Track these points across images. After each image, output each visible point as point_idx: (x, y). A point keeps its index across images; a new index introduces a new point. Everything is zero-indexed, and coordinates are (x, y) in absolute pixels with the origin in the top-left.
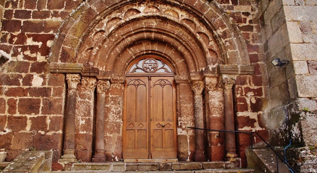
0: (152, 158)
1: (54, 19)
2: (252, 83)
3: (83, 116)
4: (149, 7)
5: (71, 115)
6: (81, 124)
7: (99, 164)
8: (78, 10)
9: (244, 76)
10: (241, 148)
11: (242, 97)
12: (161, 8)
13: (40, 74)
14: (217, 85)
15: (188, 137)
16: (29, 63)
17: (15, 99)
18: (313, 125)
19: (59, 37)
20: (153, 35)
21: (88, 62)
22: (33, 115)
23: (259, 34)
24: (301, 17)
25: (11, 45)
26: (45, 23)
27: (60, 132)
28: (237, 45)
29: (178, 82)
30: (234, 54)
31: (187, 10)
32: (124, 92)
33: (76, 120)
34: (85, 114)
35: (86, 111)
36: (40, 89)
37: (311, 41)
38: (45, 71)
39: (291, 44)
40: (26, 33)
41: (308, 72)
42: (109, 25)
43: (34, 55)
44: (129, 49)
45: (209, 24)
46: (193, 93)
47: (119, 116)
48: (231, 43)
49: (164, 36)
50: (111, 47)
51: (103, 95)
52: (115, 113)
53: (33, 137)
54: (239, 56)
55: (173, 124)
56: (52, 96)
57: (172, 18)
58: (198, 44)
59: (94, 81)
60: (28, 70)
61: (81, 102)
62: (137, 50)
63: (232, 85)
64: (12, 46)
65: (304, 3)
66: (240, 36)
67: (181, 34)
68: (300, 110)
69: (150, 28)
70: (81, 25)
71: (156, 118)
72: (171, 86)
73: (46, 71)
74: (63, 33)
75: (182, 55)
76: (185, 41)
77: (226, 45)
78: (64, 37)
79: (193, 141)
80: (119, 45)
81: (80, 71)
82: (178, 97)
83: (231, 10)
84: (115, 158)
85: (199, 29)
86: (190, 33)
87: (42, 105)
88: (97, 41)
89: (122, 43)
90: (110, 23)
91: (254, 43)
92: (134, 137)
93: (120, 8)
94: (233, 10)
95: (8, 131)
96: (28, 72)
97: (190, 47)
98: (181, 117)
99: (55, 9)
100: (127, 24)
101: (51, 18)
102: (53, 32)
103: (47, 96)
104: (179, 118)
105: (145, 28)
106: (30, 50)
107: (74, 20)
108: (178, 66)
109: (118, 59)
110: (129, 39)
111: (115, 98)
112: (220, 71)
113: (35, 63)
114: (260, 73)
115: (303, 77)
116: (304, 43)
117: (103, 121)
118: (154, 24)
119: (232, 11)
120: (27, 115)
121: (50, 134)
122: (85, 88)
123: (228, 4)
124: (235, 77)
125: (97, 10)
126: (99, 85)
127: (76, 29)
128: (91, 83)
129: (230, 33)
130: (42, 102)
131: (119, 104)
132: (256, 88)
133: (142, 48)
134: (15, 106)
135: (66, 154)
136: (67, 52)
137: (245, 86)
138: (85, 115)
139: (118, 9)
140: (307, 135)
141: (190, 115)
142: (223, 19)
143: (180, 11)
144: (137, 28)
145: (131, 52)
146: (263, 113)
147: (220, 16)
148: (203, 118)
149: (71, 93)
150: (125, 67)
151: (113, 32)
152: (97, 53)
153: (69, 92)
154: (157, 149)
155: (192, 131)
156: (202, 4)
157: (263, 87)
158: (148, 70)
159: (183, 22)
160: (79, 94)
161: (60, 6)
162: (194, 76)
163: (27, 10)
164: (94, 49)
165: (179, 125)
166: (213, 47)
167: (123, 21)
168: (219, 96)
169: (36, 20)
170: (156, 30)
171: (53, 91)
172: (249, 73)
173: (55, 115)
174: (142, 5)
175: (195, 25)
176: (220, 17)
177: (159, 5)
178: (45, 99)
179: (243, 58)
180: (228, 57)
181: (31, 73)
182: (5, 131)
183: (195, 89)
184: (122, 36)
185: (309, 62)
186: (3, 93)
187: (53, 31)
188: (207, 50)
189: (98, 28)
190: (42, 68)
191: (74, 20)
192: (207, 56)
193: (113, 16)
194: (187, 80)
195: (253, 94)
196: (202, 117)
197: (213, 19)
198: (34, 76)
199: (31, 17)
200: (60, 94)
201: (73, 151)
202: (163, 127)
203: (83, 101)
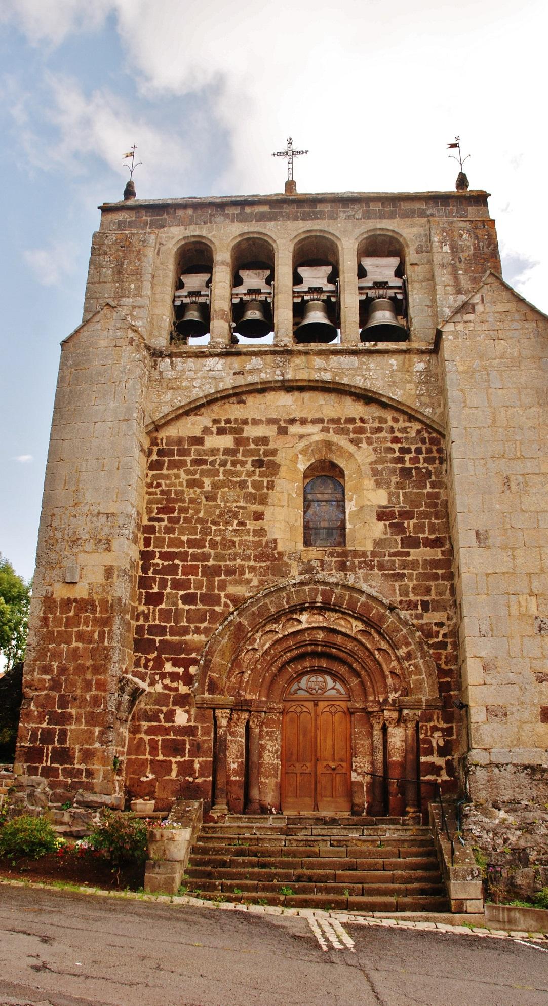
1: (196, 637)
2: (440, 720)
4: (314, 614)
6: (232, 768)
7: (256, 816)
8: (225, 626)
10: (423, 801)
12: (328, 616)
15: (365, 784)
16: (170, 695)
17: (157, 739)
20: (319, 649)
22: (179, 759)
23: (455, 653)
24: (486, 652)
26: (186, 642)
27: (211, 778)
28: (424, 670)
30: (419, 683)
31: (363, 621)
34: (236, 756)
35: (238, 752)
36: (185, 727)
37: (493, 682)
38: (190, 705)
39: (470, 687)
43: (175, 685)
44: (289, 665)
46: (372, 727)
48: (416, 667)
54: (426, 685)
57: (343, 630)
59: (245, 715)
61: (232, 741)
70: (229, 645)
74: (209, 657)
75: (358, 675)
78: (210, 661)
85: (378, 645)
87: (188, 747)
92: (295, 783)
95: (151, 776)
103: (194, 735)
104: (354, 759)
106: (170, 677)
108: (354, 689)
110: (289, 654)
111: (271, 732)
113: (176, 695)
115: (479, 726)
116: (485, 684)
119: (421, 621)
120: (171, 758)
121: (199, 780)
124: (419, 713)
128: (243, 717)
130: (188, 743)
132: (445, 726)
134: (157, 748)
135: (218, 804)
137: (432, 724)
146: (453, 759)
154: (325, 799)
155: (369, 776)
157: (454, 725)
158: (314, 691)
160: (229, 731)
163: (162, 624)
164: (246, 674)
165: (354, 768)
167: (280, 636)
168: (401, 734)
169: (173, 638)
173: (204, 759)
175: (374, 638)
176: (405, 631)
178: (192, 739)
180: (412, 686)
181: (173, 708)
182: (147, 777)
188: (387, 673)
189: (249, 645)
193: (267, 628)
195: (441, 735)
196: (382, 759)
197: (395, 634)
198: (177, 711)
201: (225, 801)
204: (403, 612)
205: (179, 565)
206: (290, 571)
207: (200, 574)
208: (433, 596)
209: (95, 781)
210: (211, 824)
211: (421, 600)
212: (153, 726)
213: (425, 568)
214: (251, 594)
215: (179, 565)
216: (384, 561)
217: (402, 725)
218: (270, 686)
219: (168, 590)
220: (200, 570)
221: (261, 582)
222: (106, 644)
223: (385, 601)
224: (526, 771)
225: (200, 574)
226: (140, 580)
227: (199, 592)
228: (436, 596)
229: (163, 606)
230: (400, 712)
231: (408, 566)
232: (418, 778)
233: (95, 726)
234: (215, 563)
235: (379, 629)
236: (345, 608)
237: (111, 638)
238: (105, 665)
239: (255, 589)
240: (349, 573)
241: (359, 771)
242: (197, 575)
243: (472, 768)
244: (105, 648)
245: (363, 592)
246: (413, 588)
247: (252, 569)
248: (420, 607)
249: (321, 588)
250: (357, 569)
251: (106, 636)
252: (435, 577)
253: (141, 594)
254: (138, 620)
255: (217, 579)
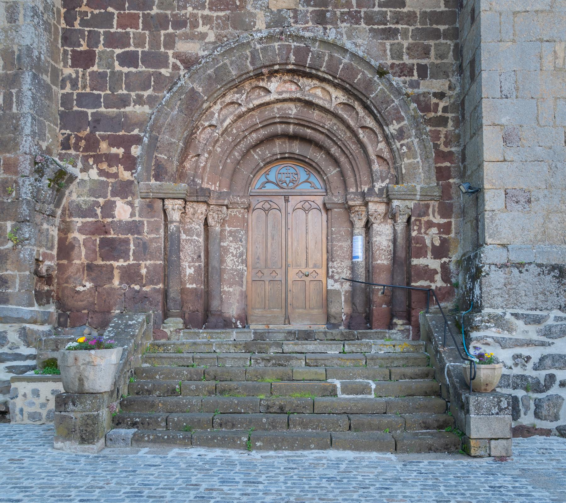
0: (289, 324)
1: (138, 109)
2: (436, 214)
3: (190, 262)
4: (285, 82)
5: (175, 261)
6: (187, 274)
9: (426, 202)
11: (421, 235)
12: (303, 84)
13: (126, 200)
14: (386, 214)
15: (343, 293)
18: (497, 283)
19: (149, 141)
20: (291, 129)
21: (194, 178)
22: (121, 263)
23: (457, 131)
25: (78, 153)
26: (125, 115)
28: (419, 151)
29: (329, 205)
30: (413, 167)
31: (344, 89)
32: (247, 222)
33: (145, 165)
34: (193, 258)
35: (195, 254)
37: (515, 158)
38: (133, 194)
39: (485, 164)
40: (97, 133)
41: (504, 207)
42: (223, 115)
43: (114, 170)
44: (255, 151)
45: (378, 115)
46: (352, 224)
47: (242, 260)
48: (409, 148)
49: (309, 131)
50: (226, 150)
51: (218, 229)
52: (236, 256)
53: (124, 293)
54: (421, 171)
55: (322, 272)
56: (146, 234)
57: (321, 103)
58: (361, 146)
59: (202, 208)
60: (107, 193)
61: (187, 241)
62: (266, 152)
63: (406, 217)
64: (79, 155)
65: (514, 95)
66: (424, 136)
67: (335, 128)
68: (483, 262)
69: (286, 118)
70: (180, 119)
71: (296, 263)
72: (320, 210)
73: (134, 195)
75: (336, 162)
76: (341, 141)
77: (402, 151)
78: (157, 139)
79: (350, 299)
80: (238, 147)
81: (185, 195)
82: (329, 231)
83: (415, 88)
84: (236, 322)
86: (348, 127)
87: (132, 247)
88: (205, 142)
89: (243, 144)
90: (224, 112)
91: (447, 147)
93: (238, 85)
94: (419, 88)
95: (89, 285)
96: (107, 196)
97: (348, 149)
98: (333, 262)
99: (138, 91)
100: (250, 112)
101: (134, 106)
102: (139, 131)
103: (139, 233)
104: (330, 264)
105: (279, 118)
107: (169, 110)
108: (331, 180)
109: (238, 169)
110: (254, 135)
111: (235, 232)
112: (388, 195)
113: (116, 183)
114: (451, 198)
115: (495, 215)
116: (505, 160)
117: (218, 268)
118: (293, 110)
119: (416, 90)
120: (112, 262)
122: (191, 219)
123: (410, 78)
125: (204, 93)
126: (211, 213)
127: (174, 126)
129: (409, 130)
131: (241, 241)
133: (274, 149)
136: (163, 164)
138: (193, 261)
139: (236, 87)
140: (487, 297)
141: (346, 259)
142: (401, 107)
143: (333, 88)
144: (266, 118)
145: (256, 155)
146: (450, 261)
147: (395, 100)
148: (364, 265)
149: (173, 229)
150: (249, 181)
151: (229, 126)
152: (206, 162)
153: (169, 226)
154: (297, 310)
155: (348, 283)
156: (367, 79)
157: (453, 220)
158: (285, 185)
159: (337, 110)
161: (144, 84)
162: (353, 200)
163: (95, 92)
165: (330, 274)
166: (383, 153)
167: (244, 109)
168: (388, 232)
169: (110, 110)
170: (296, 121)
171: (147, 225)
172: (433, 197)
174: (273, 79)
175: (357, 113)
177: (301, 78)
179: (427, 173)
180: (404, 171)
181: (113, 199)
183: (354, 219)
184: (243, 131)
185: (508, 191)
186: (75, 230)
187: (138, 129)
188: (373, 157)
190: (127, 190)
191: (169, 110)
192: (372, 167)
193: (228, 99)
194: (343, 203)
196: (364, 263)
198: (117, 203)
199: (103, 104)
200: (157, 230)
202: (307, 276)
203: (189, 239)
204: (396, 78)
205: (113, 14)
206: (255, 23)
207: (141, 26)
208: (432, 59)
209: (9, 291)
210: (163, 341)
211: (418, 64)
212: (88, 222)
213: (423, 23)
214: (206, 53)
215: (113, 14)
216: (373, 12)
217: (389, 221)
218: (233, 175)
219: (101, 48)
220: (141, 21)
221: (219, 38)
222: (14, 110)
223: (373, 62)
224: (553, 274)
225: (141, 26)
226: (63, 34)
227: (140, 50)
228: (436, 59)
229: (95, 68)
230: (388, 203)
231: (402, 19)
232: (408, 284)
233: (6, 220)
234: (159, 11)
235: (364, 99)
236: (324, 72)
237: (20, 103)
238: (15, 139)
239: (211, 47)
240: (329, 26)
241: (337, 277)
242: (137, 28)
243: (486, 268)
244: (14, 116)
245: (346, 51)
246: (408, 49)
247: (207, 20)
248: (415, 73)
249: (294, 44)
250: (339, 22)
251: (14, 100)
252: (436, 35)
253: (65, 52)
254: (63, 87)
255: (163, 32)
